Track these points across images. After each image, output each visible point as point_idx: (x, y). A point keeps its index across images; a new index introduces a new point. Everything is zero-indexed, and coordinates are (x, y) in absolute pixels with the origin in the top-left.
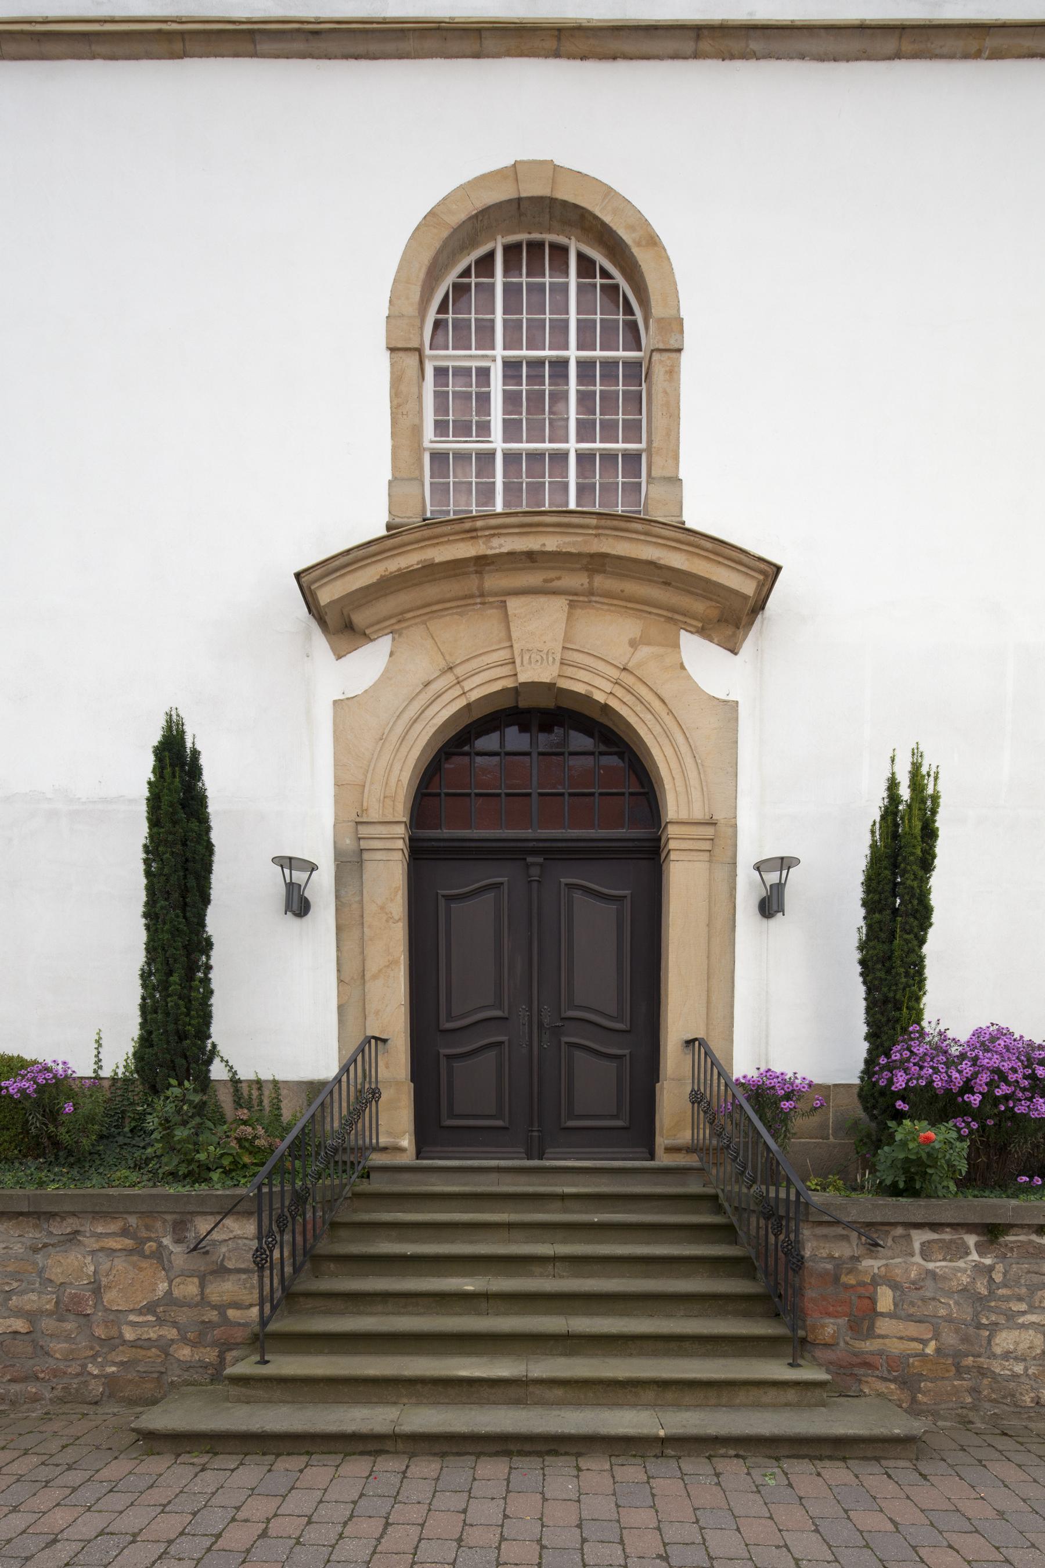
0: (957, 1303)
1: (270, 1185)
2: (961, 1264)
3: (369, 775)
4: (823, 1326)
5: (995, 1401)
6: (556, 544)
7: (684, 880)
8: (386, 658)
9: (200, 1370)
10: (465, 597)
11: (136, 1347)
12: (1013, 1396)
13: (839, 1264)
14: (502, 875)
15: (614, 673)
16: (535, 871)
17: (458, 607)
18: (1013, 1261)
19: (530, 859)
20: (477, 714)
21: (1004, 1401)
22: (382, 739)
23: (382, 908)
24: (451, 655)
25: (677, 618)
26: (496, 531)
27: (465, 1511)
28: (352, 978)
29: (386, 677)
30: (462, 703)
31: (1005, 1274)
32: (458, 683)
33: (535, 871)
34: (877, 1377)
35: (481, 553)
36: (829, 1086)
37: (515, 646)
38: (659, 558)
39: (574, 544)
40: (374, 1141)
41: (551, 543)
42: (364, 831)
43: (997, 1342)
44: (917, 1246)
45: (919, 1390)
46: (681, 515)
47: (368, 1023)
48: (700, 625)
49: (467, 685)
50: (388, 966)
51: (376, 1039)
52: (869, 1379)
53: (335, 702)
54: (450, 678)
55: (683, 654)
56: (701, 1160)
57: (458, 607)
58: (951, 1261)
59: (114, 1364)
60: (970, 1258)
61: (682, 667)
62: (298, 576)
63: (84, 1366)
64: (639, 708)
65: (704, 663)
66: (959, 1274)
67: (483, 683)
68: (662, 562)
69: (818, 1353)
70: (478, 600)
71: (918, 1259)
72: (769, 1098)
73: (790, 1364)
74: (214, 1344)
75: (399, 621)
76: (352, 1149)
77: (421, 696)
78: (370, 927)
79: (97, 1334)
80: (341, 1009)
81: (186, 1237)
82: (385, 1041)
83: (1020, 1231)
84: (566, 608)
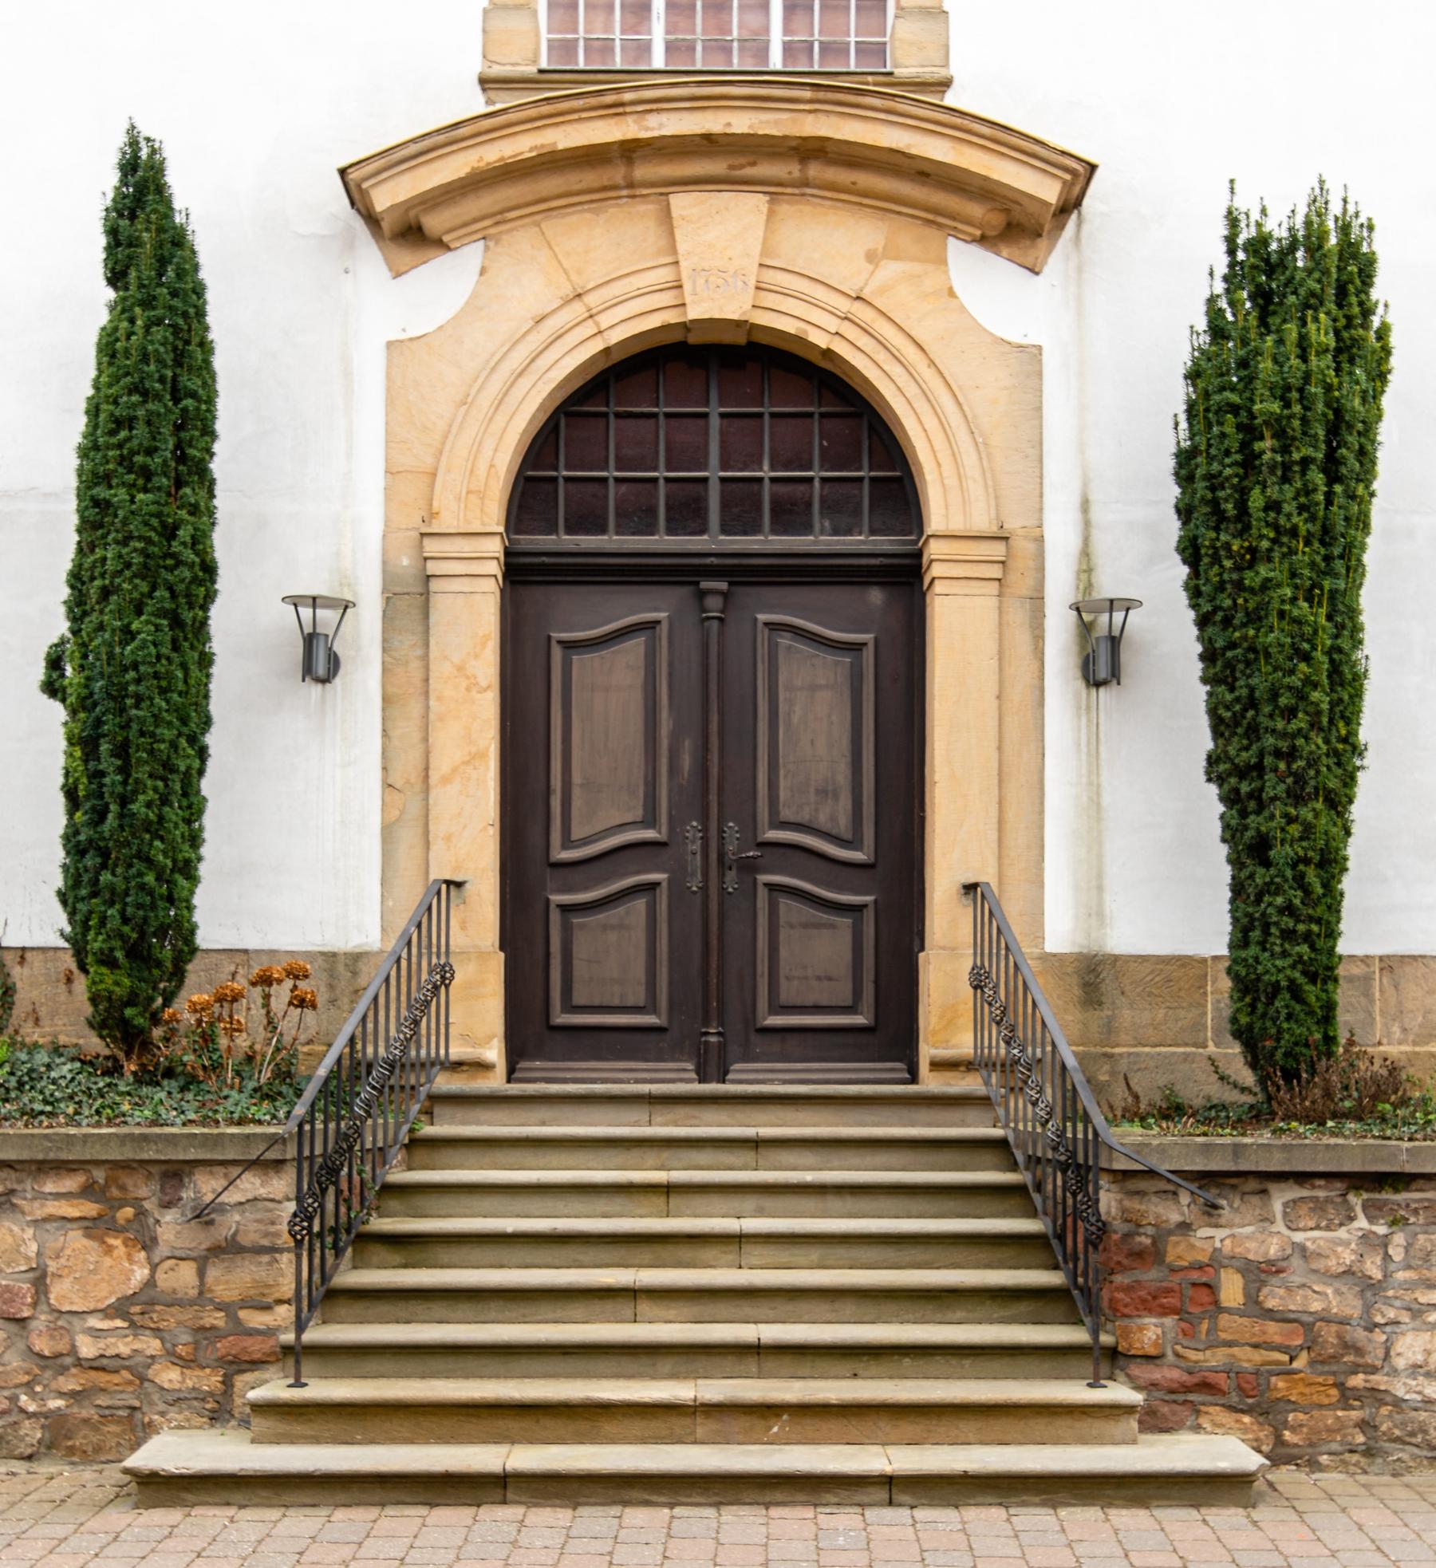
0: (1338, 1292)
1: (312, 1123)
2: (1342, 1233)
3: (444, 459)
4: (1141, 1329)
5: (1397, 1440)
6: (748, 123)
7: (960, 625)
8: (474, 276)
9: (195, 1403)
10: (604, 189)
11: (96, 1369)
12: (1425, 1432)
13: (1162, 1235)
14: (657, 607)
15: (844, 305)
16: (714, 603)
17: (592, 201)
18: (1418, 1229)
19: (705, 584)
20: (617, 357)
21: (1413, 1440)
22: (465, 402)
23: (460, 668)
24: (579, 273)
25: (938, 220)
26: (654, 106)
27: (611, 1553)
28: (408, 782)
29: (473, 307)
30: (596, 346)
31: (1408, 1248)
32: (591, 316)
33: (714, 603)
34: (1223, 1405)
35: (630, 136)
36: (1204, 961)
37: (683, 264)
38: (909, 146)
39: (776, 122)
40: (442, 1052)
41: (741, 123)
42: (432, 547)
43: (1399, 1350)
44: (1277, 1206)
45: (1285, 1424)
46: (946, 65)
47: (432, 855)
48: (978, 233)
49: (605, 320)
50: (467, 763)
51: (448, 883)
52: (1211, 1409)
53: (390, 345)
54: (577, 310)
55: (952, 274)
56: (987, 1083)
57: (592, 201)
58: (1328, 1228)
59: (61, 1394)
60: (1356, 1224)
61: (951, 293)
62: (343, 172)
63: (14, 1399)
64: (881, 356)
65: (984, 285)
66: (1340, 1249)
67: (629, 317)
68: (913, 151)
69: (1136, 1370)
70: (625, 192)
71: (1280, 1226)
72: (1093, 976)
73: (1089, 1385)
74: (222, 1362)
75: (497, 223)
76: (413, 1065)
77: (529, 338)
78: (439, 699)
79: (37, 1349)
80: (388, 833)
81: (180, 1199)
82: (460, 885)
83: (1428, 1185)
84: (765, 208)
